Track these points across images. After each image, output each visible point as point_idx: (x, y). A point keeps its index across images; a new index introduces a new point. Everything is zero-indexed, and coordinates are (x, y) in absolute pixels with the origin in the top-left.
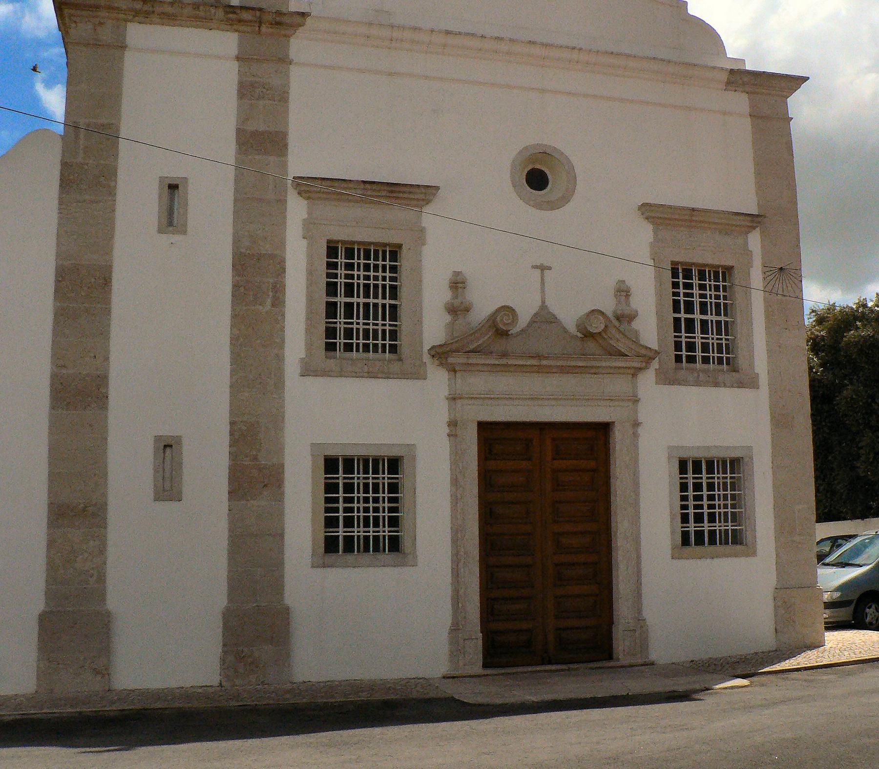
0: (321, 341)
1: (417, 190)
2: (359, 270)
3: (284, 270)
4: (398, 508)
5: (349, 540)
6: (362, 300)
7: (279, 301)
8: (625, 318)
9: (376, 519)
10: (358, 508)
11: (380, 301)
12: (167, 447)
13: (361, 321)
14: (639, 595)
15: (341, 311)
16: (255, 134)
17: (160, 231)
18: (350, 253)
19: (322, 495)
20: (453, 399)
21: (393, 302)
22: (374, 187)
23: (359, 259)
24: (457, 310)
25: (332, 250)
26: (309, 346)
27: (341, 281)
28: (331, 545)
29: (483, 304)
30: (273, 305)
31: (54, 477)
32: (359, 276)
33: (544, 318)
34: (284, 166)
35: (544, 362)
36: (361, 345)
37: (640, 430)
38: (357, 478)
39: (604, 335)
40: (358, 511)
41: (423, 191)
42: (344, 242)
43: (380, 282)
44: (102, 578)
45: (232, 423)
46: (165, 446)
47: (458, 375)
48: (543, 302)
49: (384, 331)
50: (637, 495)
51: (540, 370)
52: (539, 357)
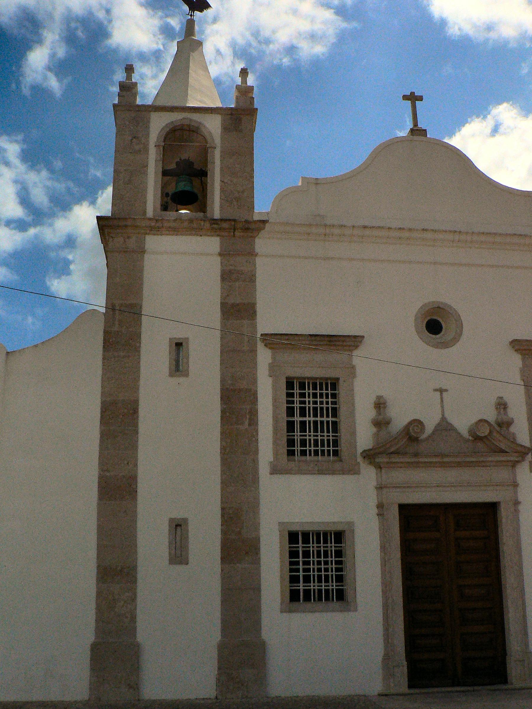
0: (284, 450)
1: (348, 339)
2: (309, 397)
3: (256, 398)
4: (342, 568)
5: (307, 593)
6: (312, 419)
7: (254, 421)
8: (505, 424)
9: (327, 577)
10: (314, 569)
11: (325, 419)
12: (178, 526)
13: (312, 433)
14: (525, 633)
15: (297, 427)
16: (233, 305)
17: (171, 375)
18: (302, 386)
19: (287, 560)
20: (380, 488)
21: (334, 419)
22: (318, 338)
23: (309, 389)
24: (381, 423)
25: (290, 384)
26: (276, 454)
27: (297, 405)
28: (294, 596)
29: (400, 417)
30: (250, 425)
31: (101, 548)
32: (309, 402)
33: (445, 427)
34: (254, 327)
35: (446, 460)
36: (312, 451)
37: (521, 507)
38: (312, 547)
39: (488, 437)
40: (314, 571)
41: (353, 339)
42: (298, 378)
43: (325, 406)
44: (133, 619)
45: (223, 509)
46: (176, 526)
47: (383, 471)
48: (443, 415)
49: (328, 441)
50: (520, 556)
51: (443, 465)
52: (443, 455)
